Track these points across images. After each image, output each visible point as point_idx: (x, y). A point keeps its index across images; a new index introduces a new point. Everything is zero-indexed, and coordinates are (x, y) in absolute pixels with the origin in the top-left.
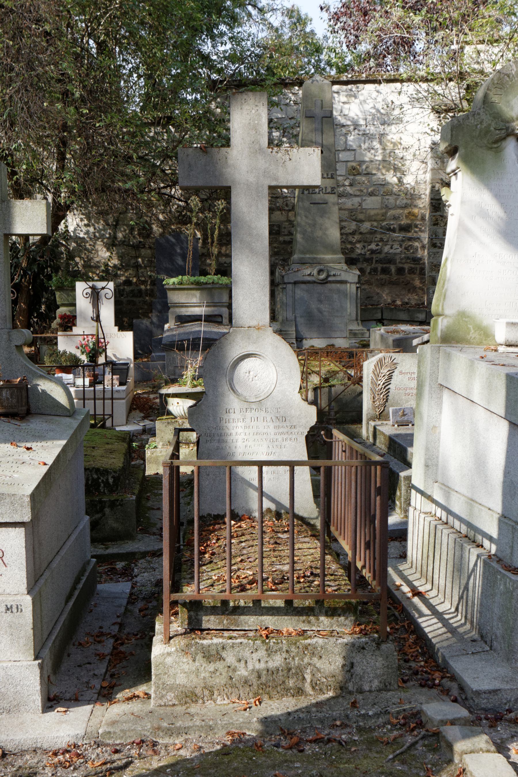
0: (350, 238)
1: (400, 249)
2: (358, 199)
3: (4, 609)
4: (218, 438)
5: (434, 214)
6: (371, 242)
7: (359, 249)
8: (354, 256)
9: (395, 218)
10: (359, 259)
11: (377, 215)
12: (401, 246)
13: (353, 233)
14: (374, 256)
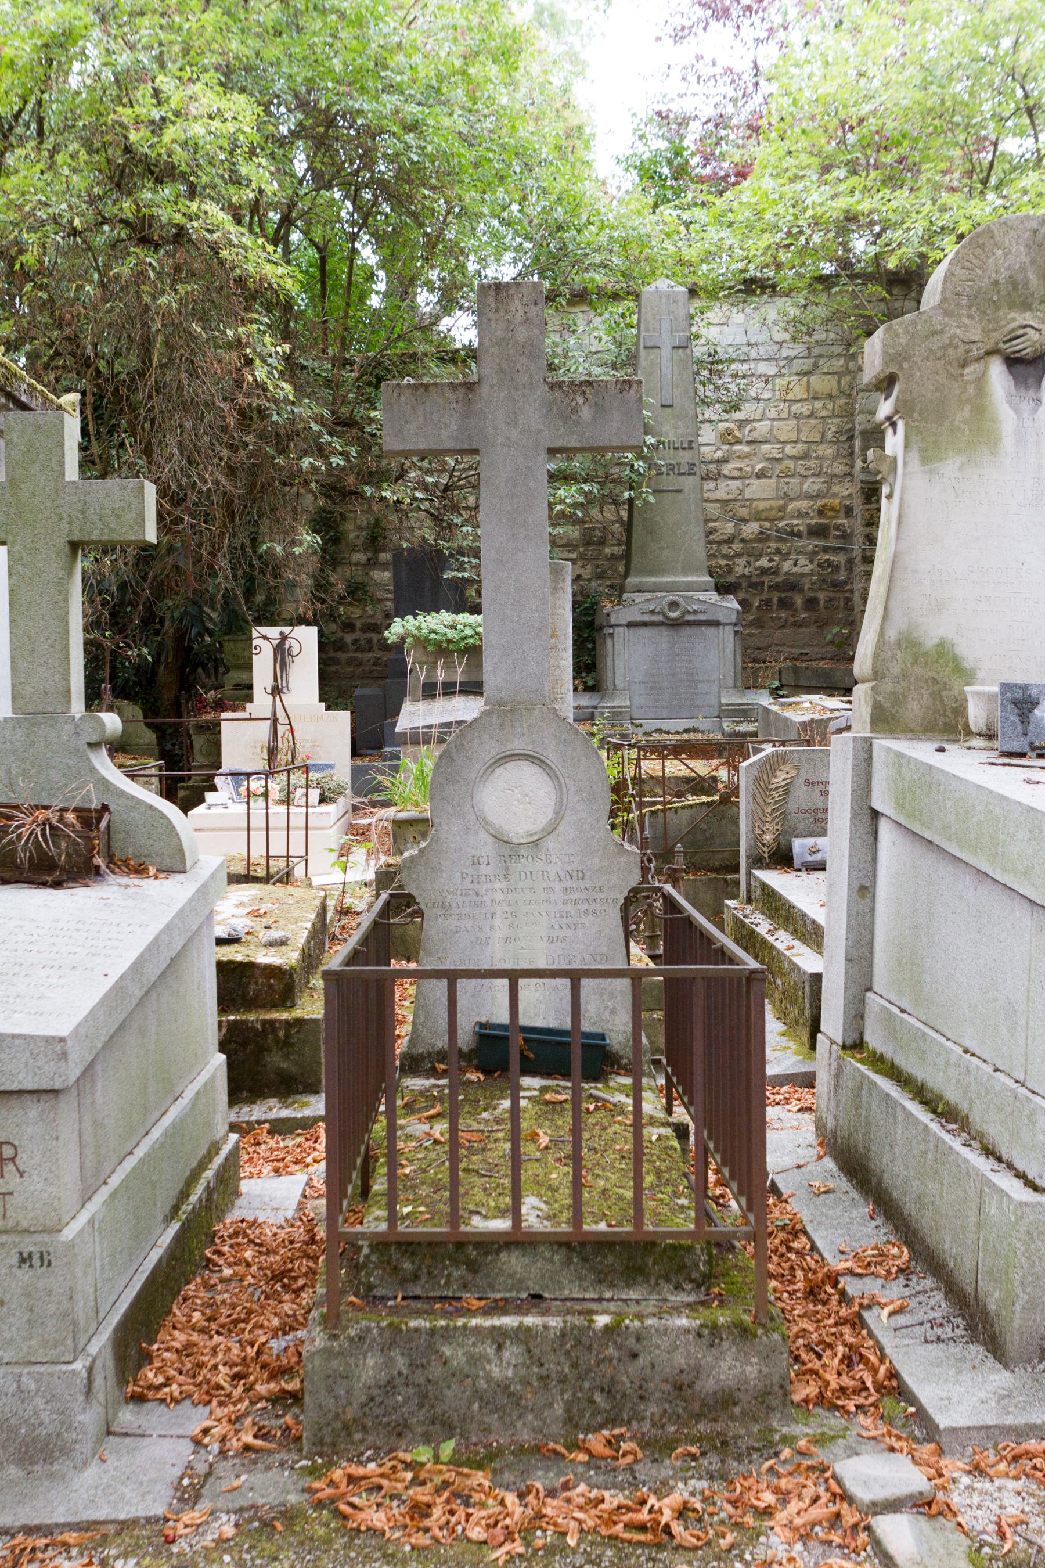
0: (725, 549)
1: (811, 567)
2: (737, 484)
3: (15, 1260)
4: (457, 912)
5: (867, 507)
6: (761, 555)
7: (741, 567)
8: (731, 579)
9: (800, 515)
10: (740, 584)
11: (771, 509)
12: (811, 561)
13: (729, 541)
14: (766, 579)
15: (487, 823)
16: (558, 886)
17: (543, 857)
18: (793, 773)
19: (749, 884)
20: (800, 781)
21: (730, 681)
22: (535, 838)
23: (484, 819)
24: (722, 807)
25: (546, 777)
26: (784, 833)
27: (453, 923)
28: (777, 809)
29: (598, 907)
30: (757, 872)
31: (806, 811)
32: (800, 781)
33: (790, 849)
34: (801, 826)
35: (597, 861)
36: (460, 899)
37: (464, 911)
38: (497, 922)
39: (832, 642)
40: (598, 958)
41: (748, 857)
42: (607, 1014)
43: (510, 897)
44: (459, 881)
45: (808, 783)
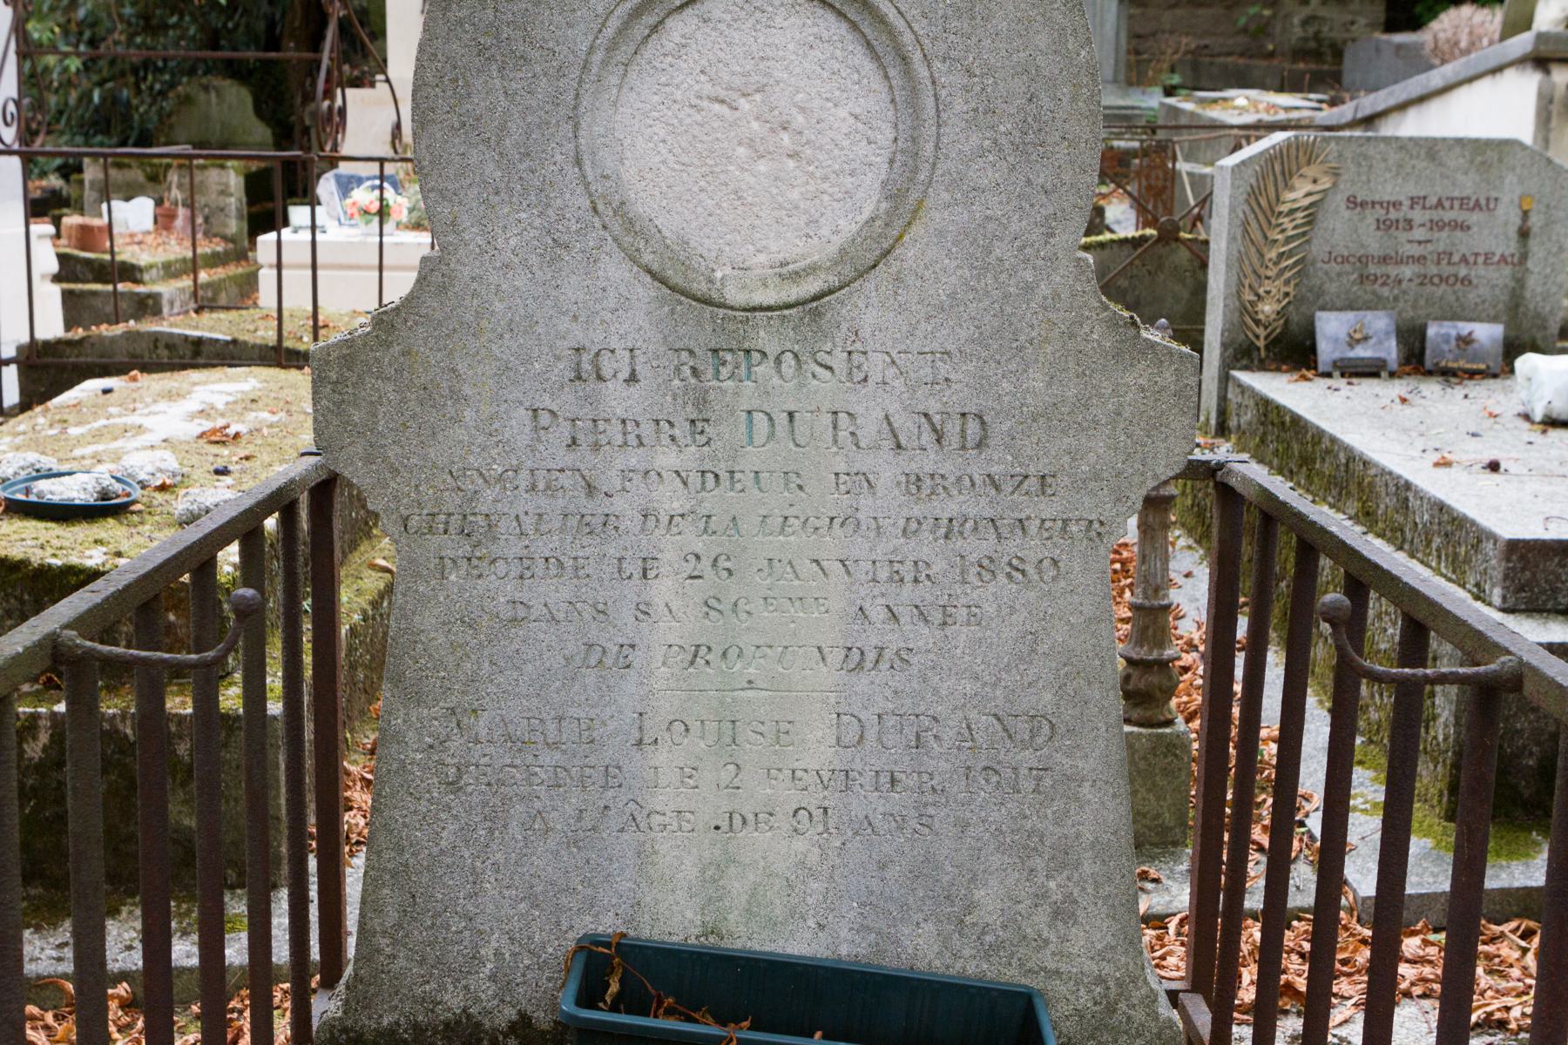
4: (516, 549)
15: (630, 224)
16: (887, 470)
17: (838, 360)
18: (1325, 183)
19: (1223, 399)
20: (1339, 200)
21: (1108, 71)
22: (812, 286)
23: (621, 209)
24: (1161, 250)
25: (860, 58)
26: (1299, 300)
27: (498, 587)
28: (1290, 254)
29: (1032, 548)
30: (1245, 377)
31: (1345, 260)
32: (1339, 200)
33: (1310, 333)
34: (1332, 288)
35: (1036, 380)
36: (526, 503)
37: (542, 548)
38: (663, 590)
39: (1245, 30)
40: (1022, 728)
41: (1224, 346)
42: (1042, 917)
43: (711, 502)
44: (523, 440)
45: (1353, 202)
